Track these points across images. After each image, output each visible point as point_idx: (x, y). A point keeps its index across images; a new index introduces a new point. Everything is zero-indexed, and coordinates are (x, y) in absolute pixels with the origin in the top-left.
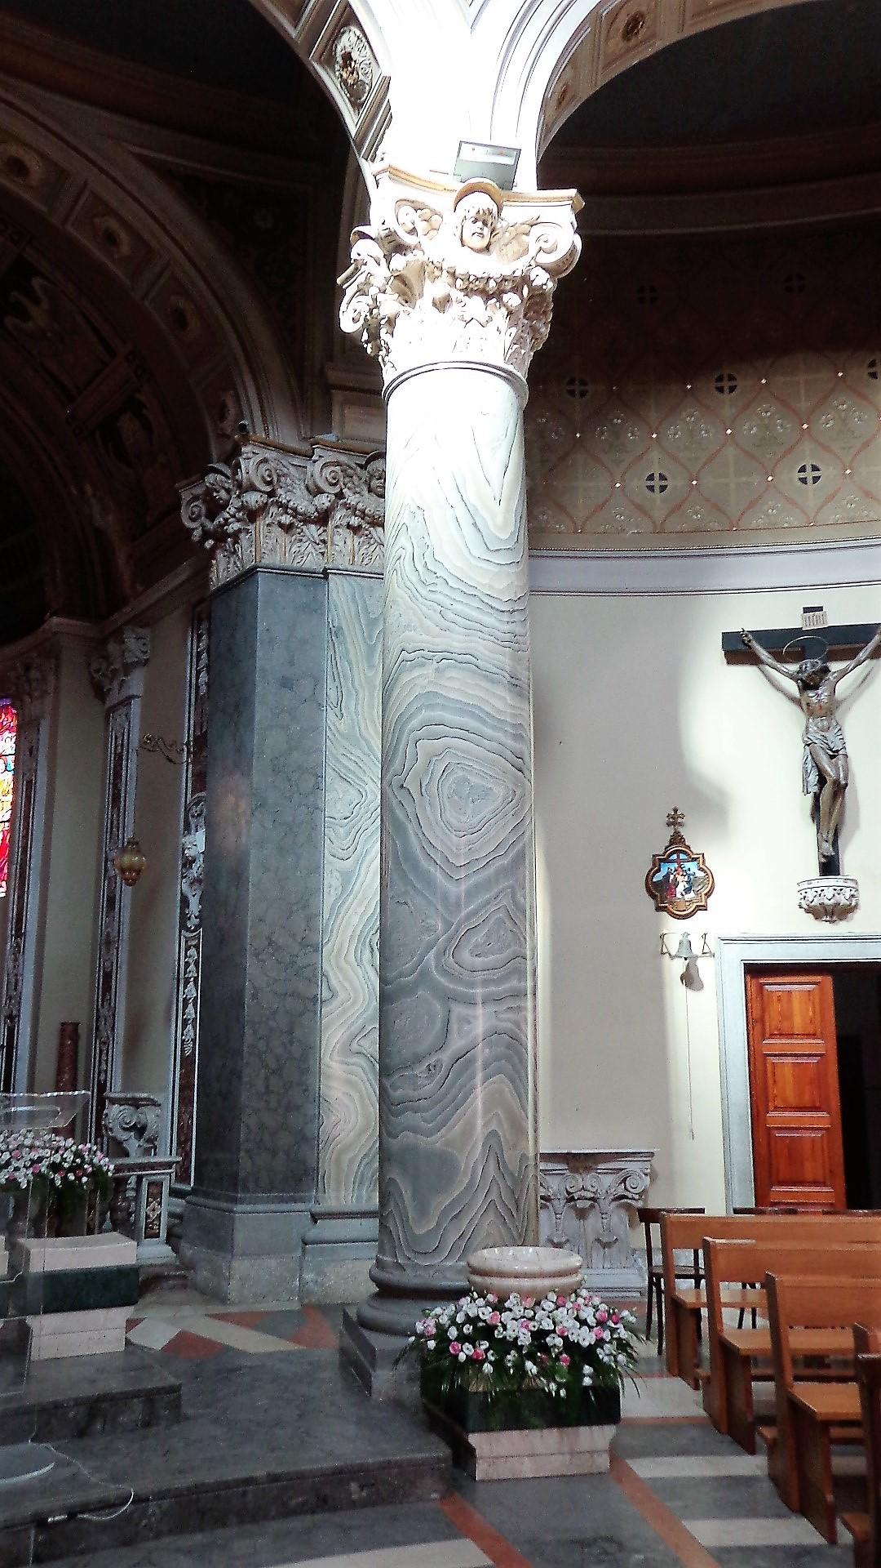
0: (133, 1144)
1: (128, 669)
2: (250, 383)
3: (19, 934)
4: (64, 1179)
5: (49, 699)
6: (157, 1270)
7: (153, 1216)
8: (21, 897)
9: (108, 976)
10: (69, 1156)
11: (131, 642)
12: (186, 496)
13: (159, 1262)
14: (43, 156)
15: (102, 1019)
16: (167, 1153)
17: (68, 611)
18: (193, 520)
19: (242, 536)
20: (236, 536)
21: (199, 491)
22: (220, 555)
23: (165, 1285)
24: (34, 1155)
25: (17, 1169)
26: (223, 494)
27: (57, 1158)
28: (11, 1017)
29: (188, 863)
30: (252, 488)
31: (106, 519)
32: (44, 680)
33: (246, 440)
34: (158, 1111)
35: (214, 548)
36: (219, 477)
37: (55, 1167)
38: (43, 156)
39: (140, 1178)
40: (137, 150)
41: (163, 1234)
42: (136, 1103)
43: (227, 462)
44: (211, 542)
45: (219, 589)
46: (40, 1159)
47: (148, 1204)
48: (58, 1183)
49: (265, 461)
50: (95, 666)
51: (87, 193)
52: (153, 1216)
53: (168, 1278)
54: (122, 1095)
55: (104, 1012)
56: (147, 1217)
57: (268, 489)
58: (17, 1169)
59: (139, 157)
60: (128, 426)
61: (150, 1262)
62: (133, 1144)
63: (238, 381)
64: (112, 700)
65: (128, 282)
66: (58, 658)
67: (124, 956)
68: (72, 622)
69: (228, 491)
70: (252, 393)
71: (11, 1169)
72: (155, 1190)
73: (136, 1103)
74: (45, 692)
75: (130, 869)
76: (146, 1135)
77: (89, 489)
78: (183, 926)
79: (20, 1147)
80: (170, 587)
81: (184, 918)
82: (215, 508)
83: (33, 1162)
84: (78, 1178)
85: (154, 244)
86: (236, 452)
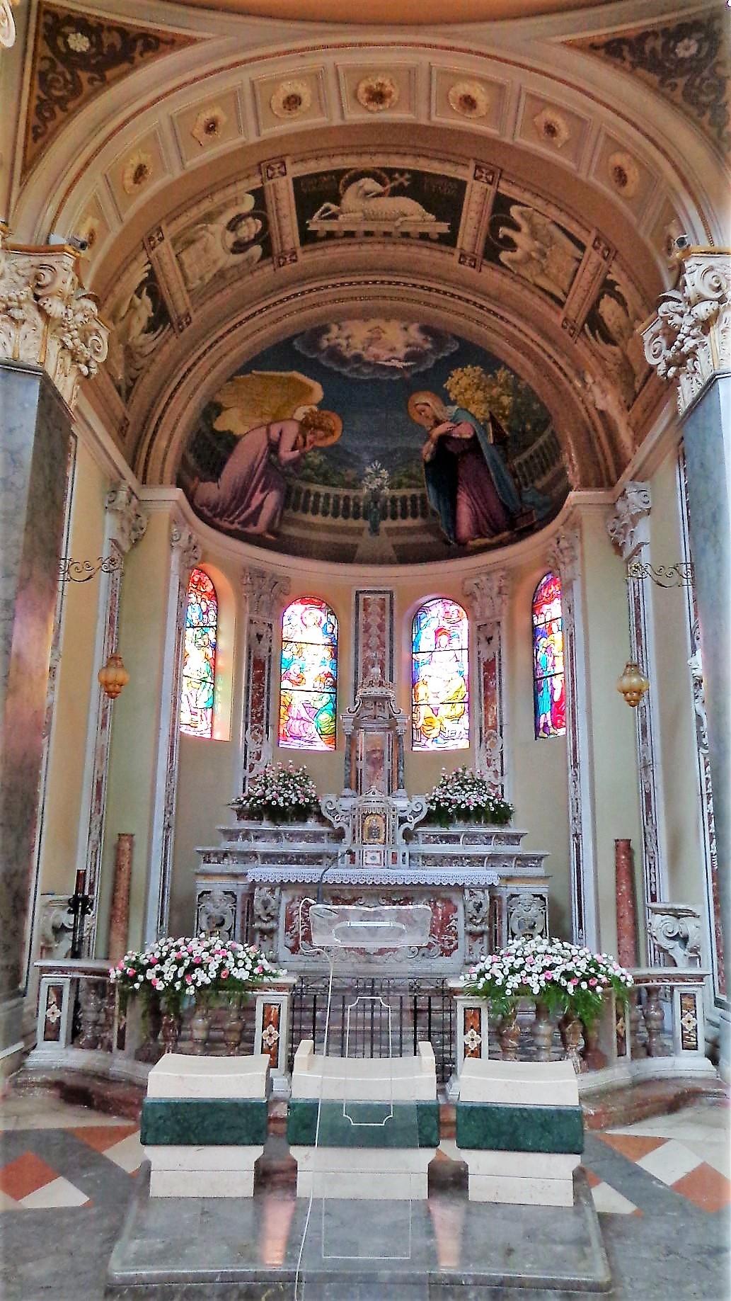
0: (679, 953)
1: (635, 519)
2: (689, 203)
3: (576, 765)
4: (577, 987)
5: (577, 564)
6: (691, 1084)
7: (689, 1028)
8: (574, 733)
9: (648, 796)
10: (583, 965)
11: (632, 495)
12: (647, 337)
13: (699, 1075)
14: (482, 81)
15: (648, 835)
16: (709, 964)
17: (585, 485)
18: (656, 356)
19: (698, 352)
20: (692, 353)
21: (658, 326)
22: (683, 379)
23: (704, 1100)
24: (547, 963)
25: (529, 974)
26: (677, 319)
27: (570, 967)
28: (576, 835)
29: (698, 683)
30: (701, 299)
31: (606, 399)
32: (572, 547)
33: (687, 253)
34: (697, 922)
35: (676, 377)
36: (671, 304)
37: (568, 975)
38: (482, 81)
39: (672, 988)
40: (564, 38)
41: (702, 1046)
42: (677, 914)
43: (676, 287)
44: (673, 369)
45: (686, 412)
46: (552, 967)
47: (682, 1015)
48: (571, 991)
49: (711, 269)
50: (611, 527)
51: (523, 99)
52: (689, 1028)
53: (708, 1094)
54: (669, 906)
55: (648, 829)
56: (683, 1028)
57: (718, 295)
58: (529, 974)
59: (570, 45)
60: (608, 308)
61: (688, 1074)
62: (679, 953)
63: (678, 209)
64: (627, 552)
65: (573, 165)
66: (580, 526)
67: (659, 777)
68: (588, 493)
69: (681, 315)
70: (693, 213)
71: (523, 973)
72: (687, 1001)
73: (677, 914)
74: (573, 559)
75: (631, 690)
76: (690, 945)
77: (589, 379)
78: (700, 744)
79: (535, 954)
80: (656, 437)
81: (700, 735)
82: (671, 334)
83: (545, 968)
84: (592, 988)
85: (584, 115)
86: (681, 270)
